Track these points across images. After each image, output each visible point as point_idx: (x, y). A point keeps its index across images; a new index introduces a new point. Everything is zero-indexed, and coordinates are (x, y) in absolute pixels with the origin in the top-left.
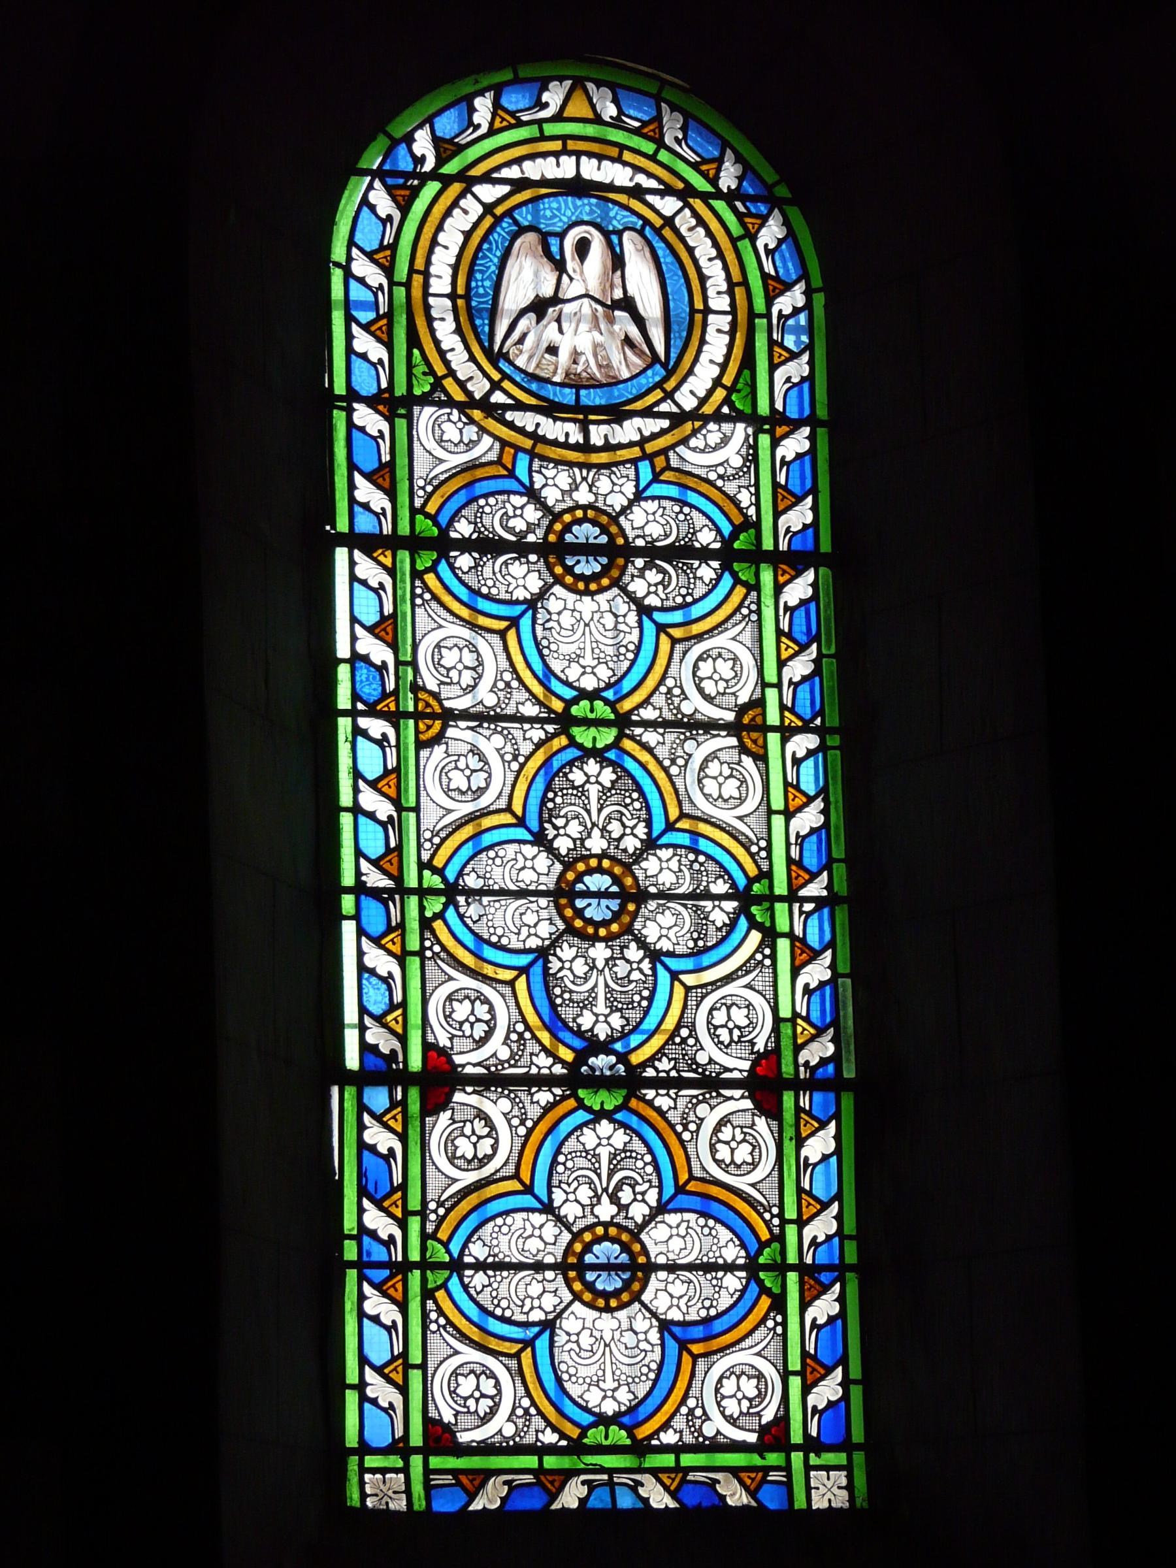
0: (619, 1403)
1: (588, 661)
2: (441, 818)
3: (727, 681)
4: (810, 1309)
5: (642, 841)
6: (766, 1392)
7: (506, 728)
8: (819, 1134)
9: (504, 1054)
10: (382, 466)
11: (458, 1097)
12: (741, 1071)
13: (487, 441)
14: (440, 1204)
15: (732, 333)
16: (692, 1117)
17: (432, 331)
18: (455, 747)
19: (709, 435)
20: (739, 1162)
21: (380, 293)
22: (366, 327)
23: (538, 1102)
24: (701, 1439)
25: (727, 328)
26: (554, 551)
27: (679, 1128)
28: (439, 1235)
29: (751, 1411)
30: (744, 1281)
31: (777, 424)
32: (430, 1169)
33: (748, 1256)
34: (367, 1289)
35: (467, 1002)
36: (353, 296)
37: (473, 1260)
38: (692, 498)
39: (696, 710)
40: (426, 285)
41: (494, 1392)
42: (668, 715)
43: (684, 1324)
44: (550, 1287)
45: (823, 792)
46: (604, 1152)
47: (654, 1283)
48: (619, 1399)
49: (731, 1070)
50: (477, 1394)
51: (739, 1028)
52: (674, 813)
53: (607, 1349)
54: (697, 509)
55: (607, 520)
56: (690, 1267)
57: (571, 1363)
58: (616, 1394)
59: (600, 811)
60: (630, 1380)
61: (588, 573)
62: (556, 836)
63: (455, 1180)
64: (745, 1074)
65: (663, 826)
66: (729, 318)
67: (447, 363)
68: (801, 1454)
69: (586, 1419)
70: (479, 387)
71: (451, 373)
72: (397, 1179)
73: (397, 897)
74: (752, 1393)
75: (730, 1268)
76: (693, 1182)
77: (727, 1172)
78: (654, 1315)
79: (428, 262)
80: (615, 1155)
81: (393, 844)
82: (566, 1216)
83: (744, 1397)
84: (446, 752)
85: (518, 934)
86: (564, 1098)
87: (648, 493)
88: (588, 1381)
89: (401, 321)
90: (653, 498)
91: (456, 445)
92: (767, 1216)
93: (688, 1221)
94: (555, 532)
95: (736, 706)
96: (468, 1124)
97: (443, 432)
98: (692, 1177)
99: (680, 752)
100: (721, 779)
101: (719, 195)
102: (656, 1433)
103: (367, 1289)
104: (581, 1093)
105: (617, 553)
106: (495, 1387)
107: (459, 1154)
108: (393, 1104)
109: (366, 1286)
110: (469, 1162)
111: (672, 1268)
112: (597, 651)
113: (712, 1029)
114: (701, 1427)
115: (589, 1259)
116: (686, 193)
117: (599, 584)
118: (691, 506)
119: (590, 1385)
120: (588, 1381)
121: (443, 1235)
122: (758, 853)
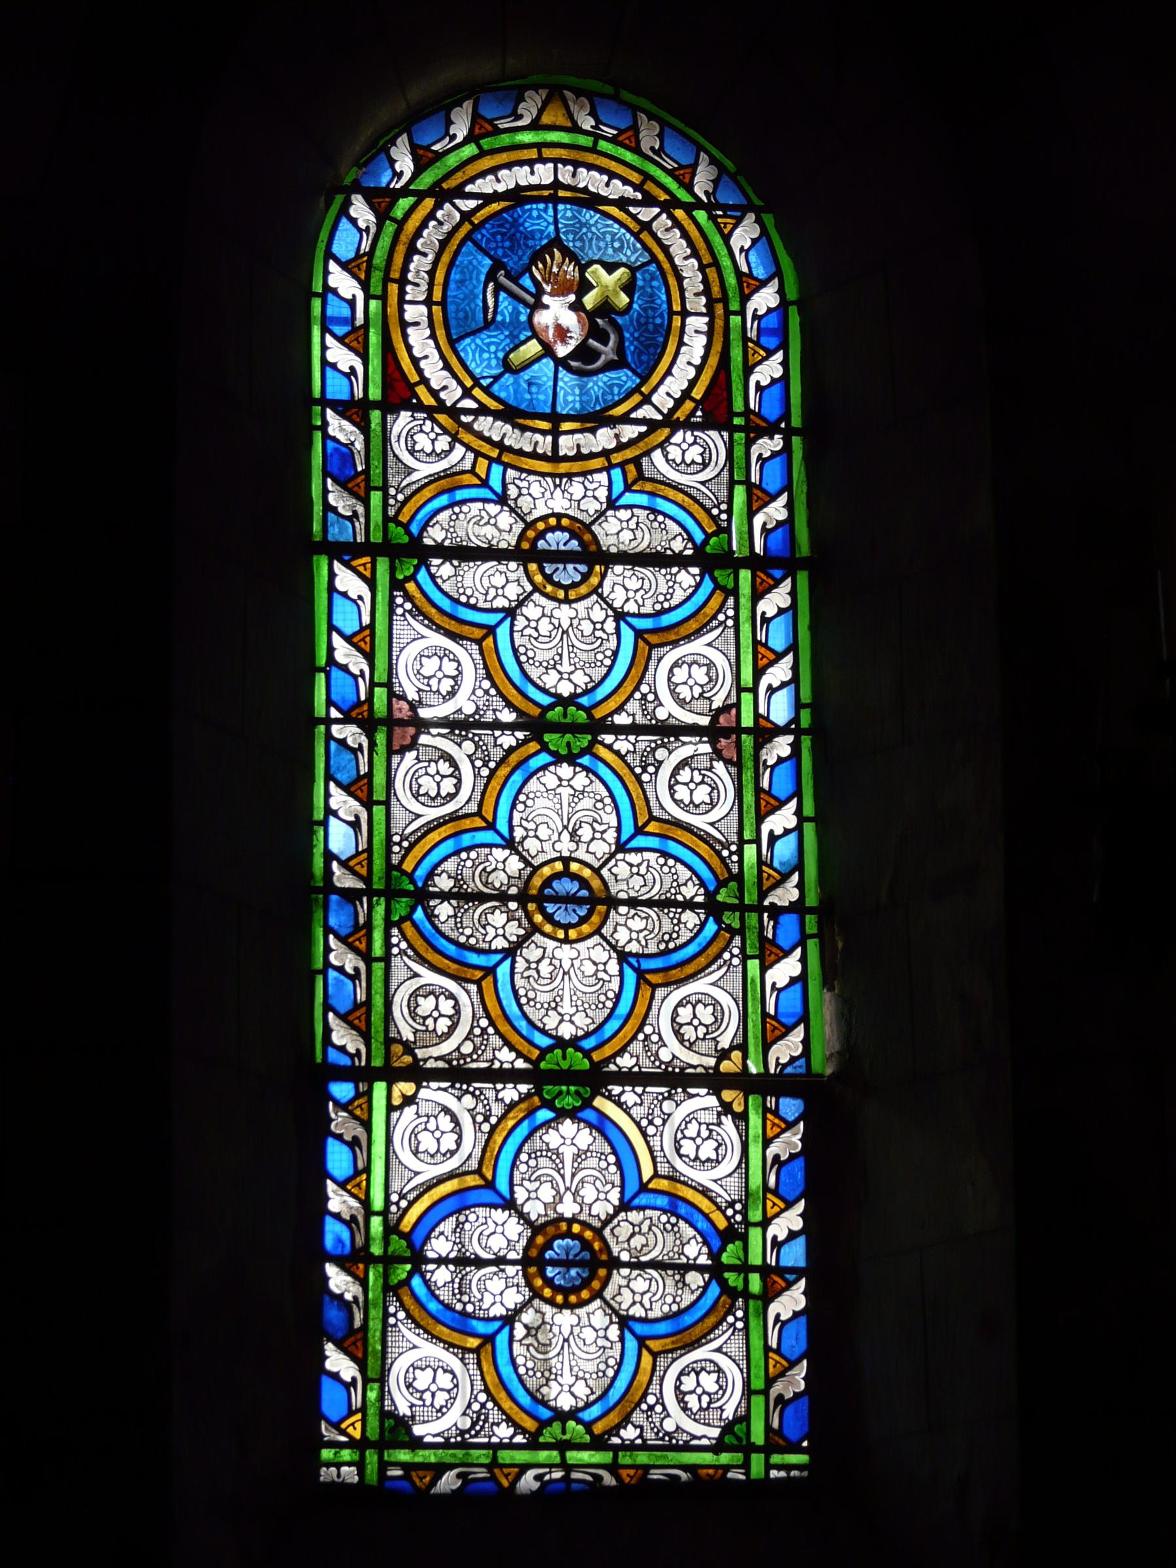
0: (577, 1027)
1: (566, 792)
2: (410, 823)
3: (427, 774)
4: (764, 677)
5: (614, 1207)
6: (722, 1020)
7: (479, 1089)
8: (783, 1215)
9: (661, 754)
10: (359, 778)
11: (715, 1433)
12: (709, 1439)
13: (459, 450)
14: (402, 1197)
15: (710, 334)
16: (657, 1112)
17: (405, 337)
18: (424, 1108)
19: (692, 1257)
20: (703, 1159)
21: (360, 680)
22: (341, 340)
23: (501, 745)
24: (654, 722)
25: (705, 328)
26: (526, 553)
27: (638, 770)
28: (404, 867)
29: (426, 764)
30: (698, 578)
31: (757, 428)
32: (394, 1163)
33: (707, 893)
34: (329, 340)
35: (432, 998)
36: (330, 312)
37: (436, 1256)
38: (673, 847)
39: (670, 715)
40: (402, 293)
41: (452, 1012)
42: (640, 719)
43: (644, 1320)
44: (512, 576)
45: (793, 647)
46: (568, 1152)
47: (617, 1279)
48: (577, 1394)
49: (699, 1438)
50: (436, 1014)
51: (709, 1394)
52: (647, 1173)
53: (566, 977)
54: (671, 518)
55: (580, 529)
56: (650, 903)
57: (529, 646)
58: (572, 677)
59: (573, 1175)
60: (586, 1006)
61: (558, 533)
62: (524, 838)
63: (418, 816)
64: (714, 1442)
65: (632, 831)
66: (706, 319)
67: (420, 372)
68: (762, 1455)
69: (545, 700)
70: (451, 395)
71: (425, 381)
72: (364, 769)
73: (365, 899)
74: (713, 1388)
75: (689, 905)
76: (653, 823)
77: (688, 811)
78: (612, 855)
79: (405, 269)
80: (579, 1156)
81: (360, 1165)
82: (528, 1213)
83: (704, 1392)
84: (417, 1113)
85: (486, 594)
86: (526, 741)
87: (622, 502)
88: (546, 1006)
89: (374, 338)
90: (626, 507)
91: (432, 1156)
92: (730, 1212)
93: (651, 1218)
94: (528, 540)
95: (711, 710)
96: (432, 1119)
97: (415, 443)
98: (656, 1175)
99: (651, 760)
100: (692, 786)
101: (699, 205)
102: (611, 714)
103: (329, 340)
104: (547, 737)
105: (595, 557)
106: (454, 1007)
107: (422, 792)
108: (358, 1095)
109: (328, 338)
110: (433, 799)
111: (633, 903)
112: (576, 1369)
113: (681, 1396)
114: (657, 1052)
115: (549, 1254)
116: (668, 207)
117: (579, 1297)
118: (665, 515)
119: (547, 1010)
120: (546, 1006)
121: (404, 518)
122: (733, 1216)
